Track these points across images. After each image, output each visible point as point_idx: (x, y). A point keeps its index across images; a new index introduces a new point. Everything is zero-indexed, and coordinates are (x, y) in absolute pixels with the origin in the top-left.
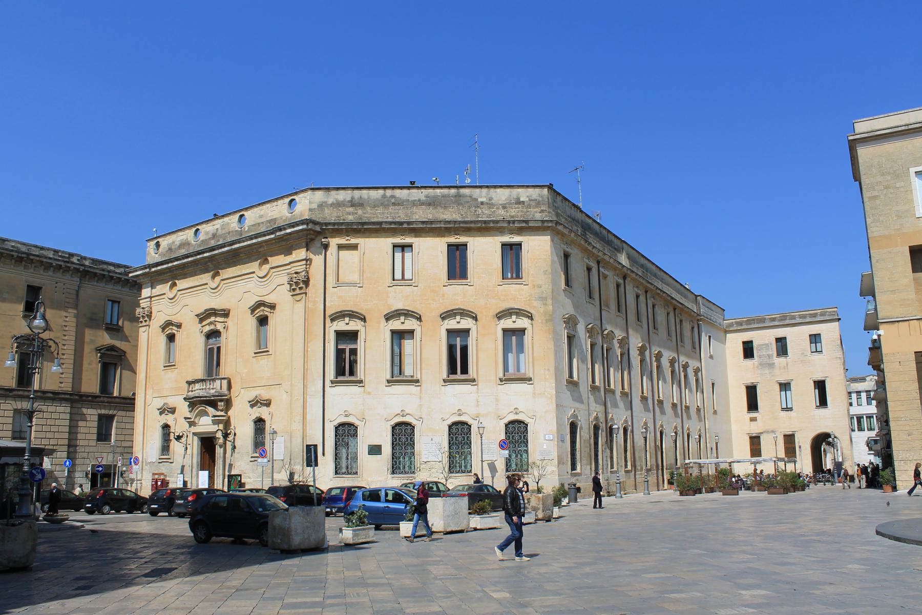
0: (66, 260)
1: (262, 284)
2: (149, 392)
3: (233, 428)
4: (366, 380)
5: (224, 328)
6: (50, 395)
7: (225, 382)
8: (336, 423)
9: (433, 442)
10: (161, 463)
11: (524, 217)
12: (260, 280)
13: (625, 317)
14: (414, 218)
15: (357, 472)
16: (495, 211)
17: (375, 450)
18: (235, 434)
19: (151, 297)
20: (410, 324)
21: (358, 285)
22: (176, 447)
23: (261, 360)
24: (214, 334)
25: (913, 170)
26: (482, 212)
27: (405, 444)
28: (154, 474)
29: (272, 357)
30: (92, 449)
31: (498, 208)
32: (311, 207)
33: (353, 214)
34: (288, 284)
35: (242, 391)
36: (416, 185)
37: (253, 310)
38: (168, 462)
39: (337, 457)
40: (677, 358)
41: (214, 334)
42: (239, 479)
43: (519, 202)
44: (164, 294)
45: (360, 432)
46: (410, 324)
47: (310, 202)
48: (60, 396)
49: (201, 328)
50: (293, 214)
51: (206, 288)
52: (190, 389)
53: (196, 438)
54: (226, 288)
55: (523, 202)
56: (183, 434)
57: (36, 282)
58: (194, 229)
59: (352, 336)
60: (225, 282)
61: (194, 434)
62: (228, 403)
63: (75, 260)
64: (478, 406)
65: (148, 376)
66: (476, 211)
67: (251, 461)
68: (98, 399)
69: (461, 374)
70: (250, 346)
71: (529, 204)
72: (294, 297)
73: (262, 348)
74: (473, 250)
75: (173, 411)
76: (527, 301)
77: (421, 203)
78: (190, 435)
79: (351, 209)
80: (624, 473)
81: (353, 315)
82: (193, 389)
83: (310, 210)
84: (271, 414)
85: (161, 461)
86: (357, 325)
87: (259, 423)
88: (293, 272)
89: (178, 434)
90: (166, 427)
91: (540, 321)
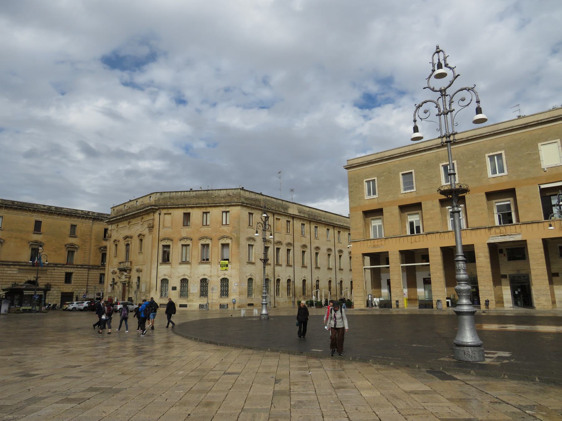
0: (86, 214)
2: (110, 266)
6: (80, 266)
7: (129, 263)
12: (142, 226)
17: (174, 288)
19: (111, 230)
20: (188, 242)
24: (128, 245)
25: (365, 180)
31: (221, 198)
36: (193, 190)
39: (161, 291)
41: (128, 245)
43: (229, 195)
44: (115, 229)
45: (169, 282)
46: (188, 242)
47: (155, 198)
48: (84, 267)
53: (121, 284)
55: (231, 195)
57: (74, 223)
58: (124, 205)
59: (168, 246)
61: (121, 282)
62: (130, 270)
63: (90, 214)
68: (100, 267)
70: (138, 250)
73: (141, 252)
77: (194, 197)
78: (119, 283)
79: (169, 200)
80: (287, 298)
81: (168, 239)
87: (139, 278)
90: (114, 279)
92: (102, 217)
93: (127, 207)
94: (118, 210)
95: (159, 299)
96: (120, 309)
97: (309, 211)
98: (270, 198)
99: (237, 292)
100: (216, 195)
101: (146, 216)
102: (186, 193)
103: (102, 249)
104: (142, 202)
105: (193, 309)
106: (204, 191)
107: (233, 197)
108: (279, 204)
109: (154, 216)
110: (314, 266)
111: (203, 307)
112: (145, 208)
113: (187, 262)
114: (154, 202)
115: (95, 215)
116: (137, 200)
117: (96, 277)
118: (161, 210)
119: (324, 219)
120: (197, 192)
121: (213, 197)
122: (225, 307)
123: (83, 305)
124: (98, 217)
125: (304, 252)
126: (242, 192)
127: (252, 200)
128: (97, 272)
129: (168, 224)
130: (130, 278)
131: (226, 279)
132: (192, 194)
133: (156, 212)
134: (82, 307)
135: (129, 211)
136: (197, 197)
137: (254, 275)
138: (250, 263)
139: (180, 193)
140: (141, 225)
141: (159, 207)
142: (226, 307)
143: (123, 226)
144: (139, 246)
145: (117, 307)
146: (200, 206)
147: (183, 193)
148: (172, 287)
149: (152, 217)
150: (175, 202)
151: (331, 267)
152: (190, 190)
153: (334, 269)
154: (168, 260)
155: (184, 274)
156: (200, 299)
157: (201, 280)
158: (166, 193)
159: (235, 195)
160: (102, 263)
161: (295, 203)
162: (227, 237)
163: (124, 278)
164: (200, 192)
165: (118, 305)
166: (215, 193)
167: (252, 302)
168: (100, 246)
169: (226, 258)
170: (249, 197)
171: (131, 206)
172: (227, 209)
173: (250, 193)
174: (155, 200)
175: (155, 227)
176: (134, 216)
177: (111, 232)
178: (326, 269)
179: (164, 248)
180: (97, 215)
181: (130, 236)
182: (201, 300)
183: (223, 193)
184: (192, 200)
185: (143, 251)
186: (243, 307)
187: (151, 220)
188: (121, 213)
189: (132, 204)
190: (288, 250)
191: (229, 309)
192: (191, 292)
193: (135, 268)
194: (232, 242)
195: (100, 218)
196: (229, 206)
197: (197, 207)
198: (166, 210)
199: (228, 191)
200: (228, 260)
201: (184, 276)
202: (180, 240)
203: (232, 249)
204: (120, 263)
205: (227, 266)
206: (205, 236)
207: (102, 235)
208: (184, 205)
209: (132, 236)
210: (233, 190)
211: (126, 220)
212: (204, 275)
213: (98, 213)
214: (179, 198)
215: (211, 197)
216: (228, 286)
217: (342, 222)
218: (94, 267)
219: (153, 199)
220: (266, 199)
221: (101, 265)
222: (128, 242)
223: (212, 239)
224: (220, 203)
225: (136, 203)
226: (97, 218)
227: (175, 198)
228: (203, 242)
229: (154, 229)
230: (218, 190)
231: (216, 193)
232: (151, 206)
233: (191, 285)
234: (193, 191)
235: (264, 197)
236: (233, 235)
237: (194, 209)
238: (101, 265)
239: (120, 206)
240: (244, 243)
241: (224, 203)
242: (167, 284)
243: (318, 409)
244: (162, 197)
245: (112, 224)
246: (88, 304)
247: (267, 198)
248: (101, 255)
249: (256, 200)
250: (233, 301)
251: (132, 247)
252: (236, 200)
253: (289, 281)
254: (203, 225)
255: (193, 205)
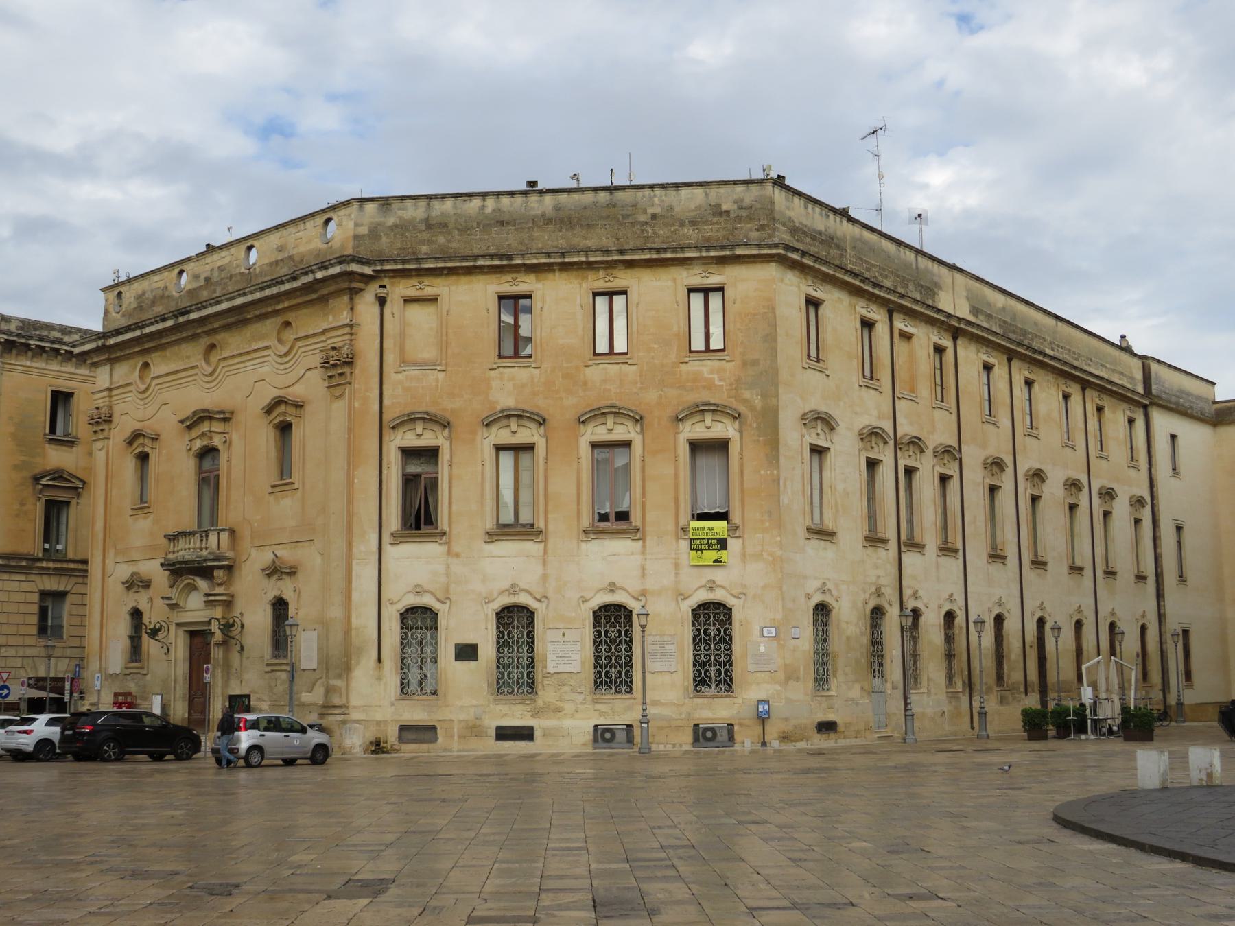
1: (282, 367)
2: (111, 553)
3: (239, 615)
4: (454, 532)
5: (225, 442)
7: (225, 536)
8: (402, 606)
9: (565, 639)
10: (129, 674)
11: (728, 239)
12: (280, 360)
13: (954, 410)
14: (535, 246)
15: (436, 691)
16: (676, 230)
17: (467, 652)
18: (242, 626)
19: (110, 389)
20: (526, 434)
21: (439, 368)
22: (150, 646)
23: (283, 498)
24: (208, 453)
26: (655, 233)
27: (615, 641)
28: (116, 695)
29: (299, 494)
30: (29, 652)
31: (682, 224)
32: (357, 233)
33: (430, 242)
34: (322, 367)
35: (253, 551)
36: (540, 187)
37: (269, 410)
38: (139, 673)
40: (1085, 481)
41: (208, 453)
42: (247, 703)
43: (719, 212)
44: (131, 384)
46: (526, 434)
47: (356, 225)
49: (189, 443)
50: (330, 244)
51: (269, 355)
52: (171, 549)
53: (181, 632)
54: (227, 374)
55: (727, 212)
56: (161, 626)
58: (177, 271)
59: (431, 454)
60: (226, 363)
64: (643, 575)
65: (108, 525)
66: (642, 231)
67: (266, 672)
68: (38, 564)
69: (616, 521)
71: (738, 216)
72: (331, 389)
74: (637, 301)
75: (147, 584)
76: (732, 389)
78: (173, 628)
79: (426, 235)
82: (176, 549)
83: (356, 237)
84: (297, 591)
85: (128, 671)
86: (437, 438)
87: (280, 606)
88: (329, 347)
89: (152, 626)
90: (136, 614)
91: (755, 425)
92: (41, 340)
93: (196, 277)
94: (144, 293)
95: (393, 704)
96: (252, 748)
97: (1004, 309)
98: (873, 237)
99: (772, 667)
100: (657, 210)
101: (305, 311)
102: (506, 201)
103: (44, 481)
104: (281, 249)
105: (564, 747)
106: (596, 190)
107: (739, 219)
108: (907, 266)
109: (352, 309)
110: (1027, 558)
111: (611, 740)
112: (306, 273)
113: (524, 526)
114: (351, 244)
115: (13, 327)
116: (247, 243)
117: (23, 608)
118: (386, 281)
119: (1053, 350)
120: (563, 197)
121: (642, 218)
122: (719, 738)
123: (31, 731)
124: (24, 337)
125: (993, 490)
126: (779, 195)
127: (814, 238)
128: (25, 586)
129: (421, 343)
130: (229, 604)
131: (719, 606)
132: (536, 205)
133: (361, 290)
134: (26, 743)
135: (205, 295)
136: (562, 221)
137: (835, 593)
138: (823, 534)
139: (477, 202)
140: (141, 393)
141: (379, 268)
142: (724, 736)
143: (173, 367)
144: (273, 454)
145: (238, 740)
146: (582, 262)
147: (490, 203)
148: (457, 645)
149: (345, 317)
150: (457, 243)
151: (1078, 563)
152: (524, 187)
153: (1088, 572)
154: (430, 521)
155: (513, 585)
156: (595, 702)
157: (596, 615)
158: (409, 203)
159: (748, 213)
160: (47, 546)
161: (961, 271)
162: (718, 410)
163: (202, 605)
164: (576, 196)
165: (239, 729)
166: (651, 198)
167: (831, 717)
168: (37, 471)
169: (706, 511)
170: (805, 222)
171: (216, 274)
172: (713, 280)
173: (806, 207)
174: (356, 237)
175: (359, 363)
176: (239, 318)
177: (110, 397)
178: (1065, 569)
179: (406, 464)
180: (17, 328)
181: (219, 412)
182: (599, 707)
183: (690, 201)
184: (536, 233)
185: (296, 477)
186: (802, 740)
187: (338, 328)
188: (159, 309)
189: (219, 263)
190: (944, 479)
191: (737, 747)
192: (550, 669)
193: (255, 560)
194: (741, 432)
195: (31, 342)
196: (722, 261)
197: (565, 267)
198: (414, 281)
199: (713, 191)
200: (723, 516)
201: (514, 593)
202: (487, 425)
203: (742, 466)
204: (173, 538)
205: (722, 544)
206: (609, 403)
207: (43, 419)
208: (501, 257)
209: (232, 413)
210: (740, 189)
211: (195, 337)
212: (612, 588)
213: (23, 321)
214: (475, 225)
215: (630, 220)
216: (728, 641)
217: (1108, 366)
218: (13, 563)
219: (340, 233)
220: (861, 239)
221: (41, 555)
222: (211, 438)
223: (641, 418)
224: (682, 249)
225: (242, 254)
226: (23, 341)
227: (451, 225)
228: (600, 433)
229: (357, 371)
230: (663, 186)
231: (656, 199)
232: (342, 260)
233: (552, 635)
234: (541, 192)
235: (857, 230)
236: (745, 401)
237: (550, 276)
238: (41, 555)
239: (156, 278)
240: (794, 438)
241: (699, 249)
242: (429, 634)
243: (644, 546)
244: (391, 221)
245: (112, 361)
246: (57, 729)
247: (867, 235)
248: (40, 507)
249: (829, 240)
250: (761, 708)
251: (233, 464)
252: (754, 235)
253: (950, 616)
254: (595, 354)
255: (548, 255)
